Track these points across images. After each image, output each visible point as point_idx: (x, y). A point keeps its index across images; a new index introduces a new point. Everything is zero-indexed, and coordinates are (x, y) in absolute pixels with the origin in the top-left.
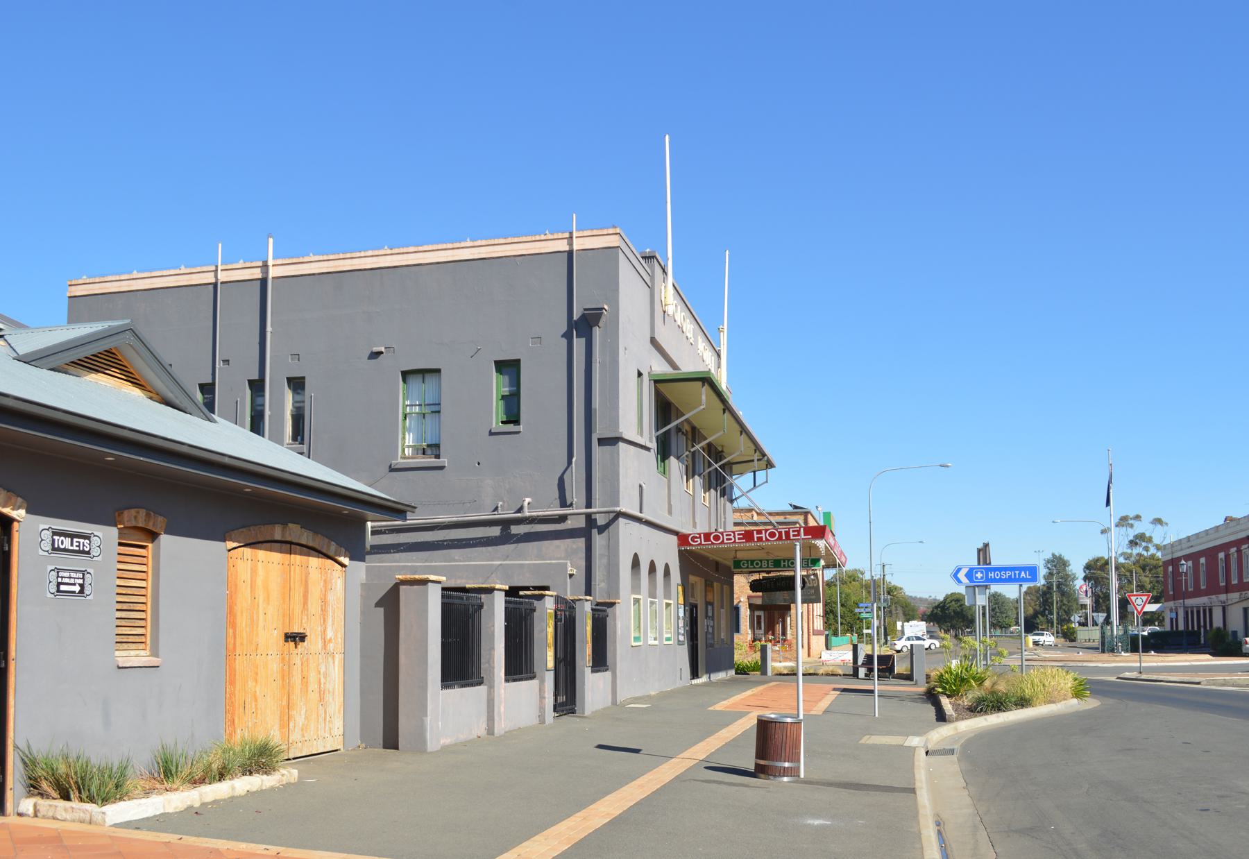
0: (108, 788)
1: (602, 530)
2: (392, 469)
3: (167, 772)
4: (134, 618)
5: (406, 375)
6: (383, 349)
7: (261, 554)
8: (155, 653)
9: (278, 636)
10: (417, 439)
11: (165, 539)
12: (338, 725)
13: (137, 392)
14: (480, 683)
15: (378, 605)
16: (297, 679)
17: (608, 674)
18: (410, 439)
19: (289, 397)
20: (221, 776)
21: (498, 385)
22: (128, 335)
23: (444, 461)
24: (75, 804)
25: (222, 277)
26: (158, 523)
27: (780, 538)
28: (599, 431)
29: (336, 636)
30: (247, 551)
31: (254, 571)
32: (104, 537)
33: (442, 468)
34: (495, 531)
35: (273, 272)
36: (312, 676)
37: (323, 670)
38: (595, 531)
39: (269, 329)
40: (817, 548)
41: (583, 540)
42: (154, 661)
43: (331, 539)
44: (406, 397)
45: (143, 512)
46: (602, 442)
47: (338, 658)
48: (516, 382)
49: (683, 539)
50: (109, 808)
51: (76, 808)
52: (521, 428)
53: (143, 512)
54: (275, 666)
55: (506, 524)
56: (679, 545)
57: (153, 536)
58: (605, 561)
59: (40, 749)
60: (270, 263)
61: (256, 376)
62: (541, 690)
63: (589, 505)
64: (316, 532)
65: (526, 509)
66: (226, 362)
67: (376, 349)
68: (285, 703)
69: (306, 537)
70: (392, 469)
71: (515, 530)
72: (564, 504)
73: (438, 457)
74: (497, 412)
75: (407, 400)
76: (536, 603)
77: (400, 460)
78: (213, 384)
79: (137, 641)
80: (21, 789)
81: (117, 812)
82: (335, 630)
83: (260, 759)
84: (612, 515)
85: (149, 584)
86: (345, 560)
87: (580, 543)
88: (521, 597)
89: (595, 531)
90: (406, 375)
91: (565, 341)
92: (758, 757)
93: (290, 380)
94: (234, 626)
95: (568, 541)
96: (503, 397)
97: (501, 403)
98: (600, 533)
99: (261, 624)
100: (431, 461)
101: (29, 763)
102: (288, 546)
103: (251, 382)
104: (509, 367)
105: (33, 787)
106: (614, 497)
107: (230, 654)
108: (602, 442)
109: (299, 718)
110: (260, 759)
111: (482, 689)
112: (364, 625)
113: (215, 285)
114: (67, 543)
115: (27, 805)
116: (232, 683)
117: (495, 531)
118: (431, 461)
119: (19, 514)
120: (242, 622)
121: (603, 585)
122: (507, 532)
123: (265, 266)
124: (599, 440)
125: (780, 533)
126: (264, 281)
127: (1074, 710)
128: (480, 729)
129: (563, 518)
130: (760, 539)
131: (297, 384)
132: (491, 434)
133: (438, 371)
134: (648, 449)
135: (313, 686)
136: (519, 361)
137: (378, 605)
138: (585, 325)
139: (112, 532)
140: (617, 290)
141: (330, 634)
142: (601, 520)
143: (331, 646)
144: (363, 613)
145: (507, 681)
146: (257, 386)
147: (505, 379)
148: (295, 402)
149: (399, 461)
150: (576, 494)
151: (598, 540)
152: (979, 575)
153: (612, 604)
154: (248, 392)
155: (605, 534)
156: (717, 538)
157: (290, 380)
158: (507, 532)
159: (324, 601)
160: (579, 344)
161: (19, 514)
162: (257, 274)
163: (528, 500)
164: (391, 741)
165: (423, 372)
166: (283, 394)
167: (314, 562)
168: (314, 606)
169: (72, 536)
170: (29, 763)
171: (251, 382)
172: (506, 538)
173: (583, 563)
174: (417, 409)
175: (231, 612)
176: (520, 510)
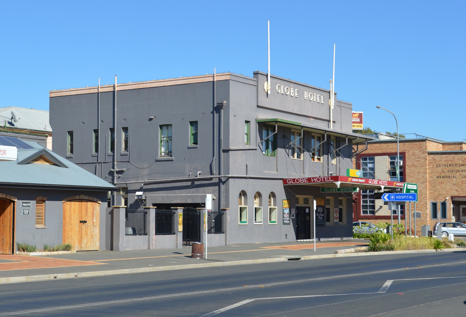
0: (34, 250)
1: (224, 183)
2: (156, 161)
3: (45, 249)
4: (40, 218)
5: (161, 127)
6: (153, 117)
7: (73, 203)
8: (45, 225)
9: (77, 221)
10: (165, 150)
11: (46, 202)
12: (98, 244)
13: (47, 164)
14: (223, 233)
15: (109, 214)
16: (84, 232)
17: (222, 235)
18: (163, 149)
19: (123, 134)
20: (57, 251)
21: (190, 130)
22: (44, 152)
23: (173, 158)
24: (26, 252)
25: (100, 90)
26: (45, 198)
27: (321, 181)
28: (223, 147)
29: (97, 222)
30: (69, 203)
31: (71, 207)
32: (33, 203)
33: (172, 160)
34: (189, 183)
35: (117, 89)
36: (89, 231)
37: (92, 230)
38: (221, 184)
39: (116, 110)
40: (336, 185)
41: (376, 157)
42: (44, 227)
43: (95, 197)
44: (162, 134)
45: (41, 197)
46: (224, 151)
47: (98, 227)
48: (196, 129)
49: (285, 181)
50: (31, 253)
51: (26, 253)
52: (198, 146)
53: (41, 197)
54: (77, 229)
55: (193, 181)
56: (284, 184)
57: (44, 201)
58: (225, 194)
59: (20, 243)
60: (116, 86)
61: (112, 127)
62: (177, 238)
63: (219, 175)
64: (89, 196)
65: (198, 176)
66: (102, 121)
67: (151, 117)
68: (80, 237)
69: (86, 198)
70: (156, 161)
71: (196, 183)
72: (212, 174)
73: (171, 156)
74: (191, 139)
75: (161, 136)
76: (175, 211)
77: (159, 158)
78: (98, 130)
79: (41, 223)
80: (17, 250)
81: (32, 254)
82: (96, 220)
83: (67, 248)
84: (227, 178)
85: (44, 211)
86: (100, 202)
87: (217, 188)
88: (172, 209)
89: (221, 184)
90: (161, 127)
91: (212, 115)
92: (192, 253)
93: (123, 128)
94: (65, 219)
95: (213, 187)
96: (193, 134)
97: (192, 136)
98: (223, 184)
99: (73, 218)
100: (169, 158)
101: (18, 245)
102: (81, 200)
103: (110, 129)
104: (194, 124)
105: (19, 250)
106: (228, 171)
107: (64, 226)
108: (224, 151)
109: (84, 241)
110: (67, 248)
111: (224, 234)
112: (106, 218)
113: (98, 93)
114: (25, 205)
115: (18, 253)
116: (65, 232)
117: (189, 183)
118: (169, 158)
119: (16, 200)
120: (67, 219)
121: (224, 203)
122: (194, 184)
123: (114, 87)
124: (223, 150)
125: (321, 179)
126: (114, 92)
127: (433, 253)
128: (146, 247)
129: (211, 179)
130: (314, 181)
131: (125, 129)
132: (188, 148)
133: (171, 125)
134: (256, 149)
135: (89, 233)
136: (197, 121)
137: (109, 214)
138: (218, 109)
139: (35, 201)
140: (229, 95)
141: (95, 221)
142: (223, 180)
143: (95, 224)
144: (106, 215)
145: (156, 235)
146: (112, 130)
147: (193, 128)
148: (125, 136)
149: (159, 158)
150: (215, 171)
151: (222, 187)
152: (393, 197)
153: (225, 210)
154: (110, 133)
155: (225, 184)
156: (297, 181)
157: (123, 128)
158: (194, 184)
159: (93, 213)
160: (216, 115)
161: (16, 200)
162: (112, 89)
163: (199, 172)
164: (112, 249)
165: (168, 126)
166: (121, 133)
167: (89, 204)
168: (90, 214)
169: (26, 203)
170: (18, 245)
171: (110, 129)
172: (193, 186)
173: (218, 195)
174: (165, 139)
175: (64, 216)
176: (196, 176)
